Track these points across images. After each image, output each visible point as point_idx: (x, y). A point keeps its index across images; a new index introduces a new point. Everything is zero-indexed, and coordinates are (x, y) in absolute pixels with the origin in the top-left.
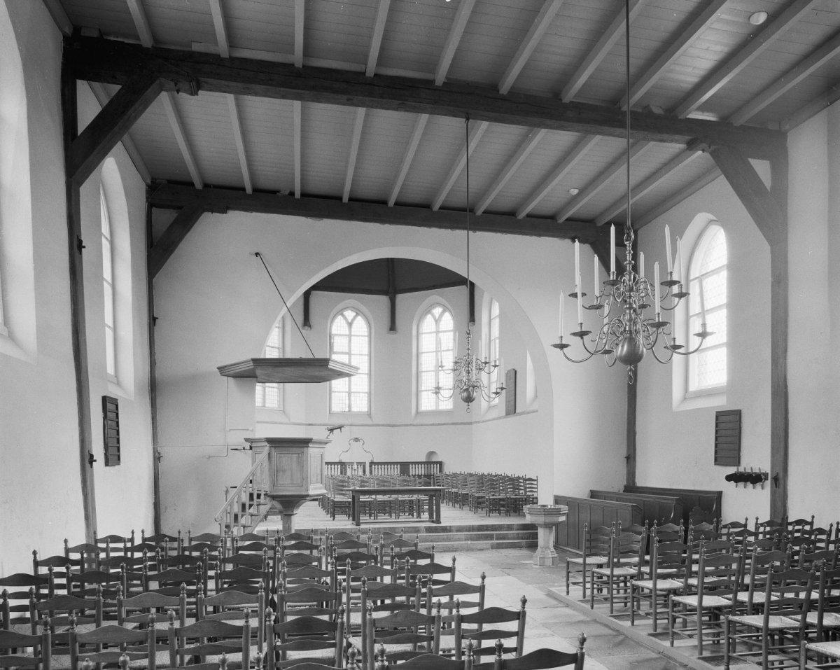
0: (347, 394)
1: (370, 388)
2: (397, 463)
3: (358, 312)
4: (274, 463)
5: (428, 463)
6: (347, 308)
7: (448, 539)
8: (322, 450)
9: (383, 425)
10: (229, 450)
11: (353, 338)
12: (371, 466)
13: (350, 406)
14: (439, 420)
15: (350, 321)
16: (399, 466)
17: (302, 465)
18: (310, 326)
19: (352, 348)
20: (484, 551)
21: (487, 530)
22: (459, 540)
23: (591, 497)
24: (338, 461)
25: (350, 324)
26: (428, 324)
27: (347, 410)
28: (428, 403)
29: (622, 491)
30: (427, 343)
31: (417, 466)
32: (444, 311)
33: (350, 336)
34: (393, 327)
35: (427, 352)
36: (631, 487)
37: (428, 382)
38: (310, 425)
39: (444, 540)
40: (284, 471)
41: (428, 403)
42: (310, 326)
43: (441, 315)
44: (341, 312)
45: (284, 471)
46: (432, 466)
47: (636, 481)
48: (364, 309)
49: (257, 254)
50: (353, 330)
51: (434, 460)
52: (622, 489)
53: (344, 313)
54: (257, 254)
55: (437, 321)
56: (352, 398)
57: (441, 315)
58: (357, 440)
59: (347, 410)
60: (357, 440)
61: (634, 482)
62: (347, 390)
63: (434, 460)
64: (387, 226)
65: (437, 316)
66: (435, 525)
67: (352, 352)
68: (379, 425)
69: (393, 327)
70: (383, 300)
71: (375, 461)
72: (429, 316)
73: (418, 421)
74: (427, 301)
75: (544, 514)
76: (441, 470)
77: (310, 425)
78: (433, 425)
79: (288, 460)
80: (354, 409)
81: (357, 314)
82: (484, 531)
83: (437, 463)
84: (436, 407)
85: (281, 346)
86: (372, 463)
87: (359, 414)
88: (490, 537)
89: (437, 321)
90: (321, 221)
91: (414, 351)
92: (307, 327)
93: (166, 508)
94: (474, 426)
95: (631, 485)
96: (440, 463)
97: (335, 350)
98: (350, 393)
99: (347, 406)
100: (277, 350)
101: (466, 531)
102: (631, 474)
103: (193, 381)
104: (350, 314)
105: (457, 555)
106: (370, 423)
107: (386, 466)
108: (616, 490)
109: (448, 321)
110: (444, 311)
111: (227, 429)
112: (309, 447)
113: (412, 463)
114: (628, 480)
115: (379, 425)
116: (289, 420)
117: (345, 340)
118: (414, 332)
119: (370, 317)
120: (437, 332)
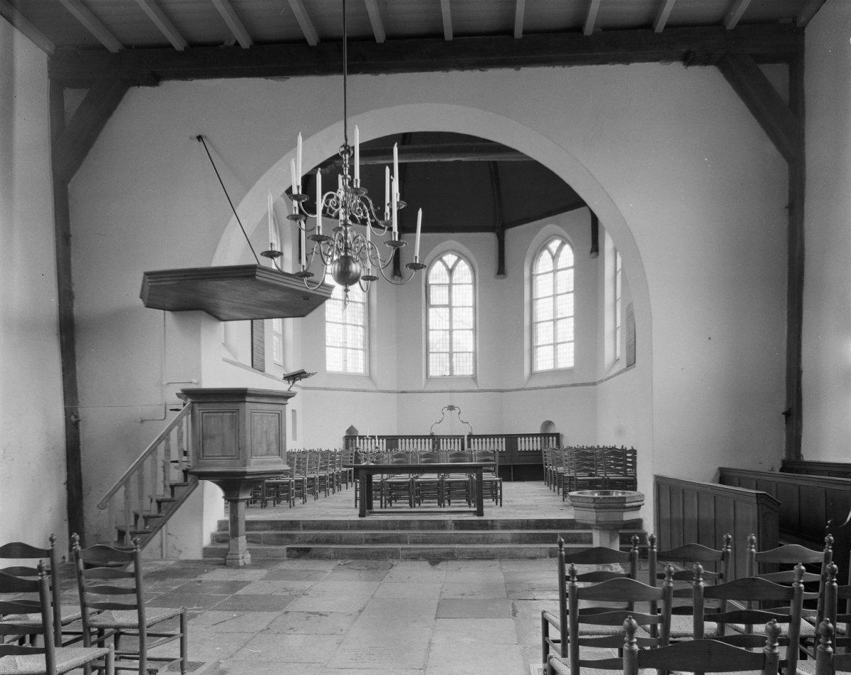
0: (448, 355)
1: (475, 348)
2: (501, 436)
3: (461, 256)
4: (199, 424)
5: (545, 436)
6: (445, 252)
7: (485, 540)
8: (281, 407)
9: (490, 391)
10: (168, 411)
11: (454, 287)
12: (469, 440)
13: (451, 369)
14: (560, 381)
15: (450, 267)
16: (504, 439)
17: (237, 425)
18: (400, 276)
19: (454, 300)
20: (538, 561)
21: (550, 527)
22: (502, 541)
23: (721, 482)
24: (429, 434)
25: (451, 272)
26: (544, 262)
27: (448, 373)
28: (544, 362)
29: (777, 471)
30: (543, 286)
31: (527, 439)
32: (563, 244)
33: (450, 285)
34: (501, 270)
35: (542, 298)
36: (794, 463)
37: (544, 334)
38: (402, 392)
39: (479, 541)
40: (212, 437)
41: (544, 362)
42: (400, 276)
43: (560, 249)
44: (439, 257)
45: (212, 437)
46: (551, 438)
47: (803, 452)
48: (466, 250)
49: (200, 138)
50: (454, 277)
51: (552, 431)
52: (779, 465)
53: (444, 258)
54: (200, 138)
55: (555, 258)
56: (454, 360)
57: (560, 249)
58: (451, 408)
59: (448, 373)
60: (451, 408)
61: (799, 455)
62: (448, 350)
63: (551, 432)
64: (382, 76)
65: (554, 251)
66: (476, 518)
67: (453, 305)
68: (485, 391)
69: (501, 270)
70: (490, 237)
71: (474, 434)
72: (546, 253)
73: (534, 383)
74: (541, 233)
75: (595, 508)
76: (558, 443)
77: (402, 392)
78: (549, 387)
79: (217, 421)
80: (457, 373)
81: (459, 259)
82: (545, 529)
83: (553, 435)
84: (554, 366)
85: (366, 301)
86: (470, 436)
87: (462, 378)
88: (551, 539)
89: (555, 258)
90: (288, 81)
91: (527, 298)
92: (396, 277)
93: (90, 489)
94: (600, 386)
95: (794, 458)
96: (558, 436)
97: (432, 303)
98: (451, 354)
99: (448, 369)
100: (341, 302)
101: (518, 528)
102: (794, 439)
103: (117, 321)
104: (450, 259)
105: (60, 632)
106: (476, 388)
107: (488, 440)
108: (765, 468)
109: (568, 256)
110: (563, 244)
111: (165, 383)
112: (245, 402)
113: (521, 436)
114: (788, 450)
115: (485, 391)
116: (375, 385)
117: (445, 291)
118: (527, 274)
119: (473, 259)
120: (555, 271)
